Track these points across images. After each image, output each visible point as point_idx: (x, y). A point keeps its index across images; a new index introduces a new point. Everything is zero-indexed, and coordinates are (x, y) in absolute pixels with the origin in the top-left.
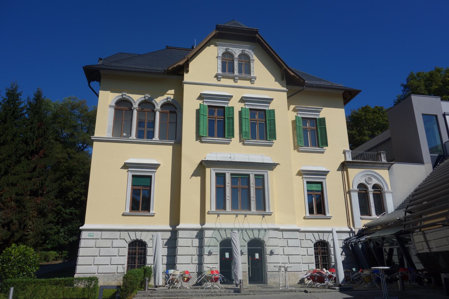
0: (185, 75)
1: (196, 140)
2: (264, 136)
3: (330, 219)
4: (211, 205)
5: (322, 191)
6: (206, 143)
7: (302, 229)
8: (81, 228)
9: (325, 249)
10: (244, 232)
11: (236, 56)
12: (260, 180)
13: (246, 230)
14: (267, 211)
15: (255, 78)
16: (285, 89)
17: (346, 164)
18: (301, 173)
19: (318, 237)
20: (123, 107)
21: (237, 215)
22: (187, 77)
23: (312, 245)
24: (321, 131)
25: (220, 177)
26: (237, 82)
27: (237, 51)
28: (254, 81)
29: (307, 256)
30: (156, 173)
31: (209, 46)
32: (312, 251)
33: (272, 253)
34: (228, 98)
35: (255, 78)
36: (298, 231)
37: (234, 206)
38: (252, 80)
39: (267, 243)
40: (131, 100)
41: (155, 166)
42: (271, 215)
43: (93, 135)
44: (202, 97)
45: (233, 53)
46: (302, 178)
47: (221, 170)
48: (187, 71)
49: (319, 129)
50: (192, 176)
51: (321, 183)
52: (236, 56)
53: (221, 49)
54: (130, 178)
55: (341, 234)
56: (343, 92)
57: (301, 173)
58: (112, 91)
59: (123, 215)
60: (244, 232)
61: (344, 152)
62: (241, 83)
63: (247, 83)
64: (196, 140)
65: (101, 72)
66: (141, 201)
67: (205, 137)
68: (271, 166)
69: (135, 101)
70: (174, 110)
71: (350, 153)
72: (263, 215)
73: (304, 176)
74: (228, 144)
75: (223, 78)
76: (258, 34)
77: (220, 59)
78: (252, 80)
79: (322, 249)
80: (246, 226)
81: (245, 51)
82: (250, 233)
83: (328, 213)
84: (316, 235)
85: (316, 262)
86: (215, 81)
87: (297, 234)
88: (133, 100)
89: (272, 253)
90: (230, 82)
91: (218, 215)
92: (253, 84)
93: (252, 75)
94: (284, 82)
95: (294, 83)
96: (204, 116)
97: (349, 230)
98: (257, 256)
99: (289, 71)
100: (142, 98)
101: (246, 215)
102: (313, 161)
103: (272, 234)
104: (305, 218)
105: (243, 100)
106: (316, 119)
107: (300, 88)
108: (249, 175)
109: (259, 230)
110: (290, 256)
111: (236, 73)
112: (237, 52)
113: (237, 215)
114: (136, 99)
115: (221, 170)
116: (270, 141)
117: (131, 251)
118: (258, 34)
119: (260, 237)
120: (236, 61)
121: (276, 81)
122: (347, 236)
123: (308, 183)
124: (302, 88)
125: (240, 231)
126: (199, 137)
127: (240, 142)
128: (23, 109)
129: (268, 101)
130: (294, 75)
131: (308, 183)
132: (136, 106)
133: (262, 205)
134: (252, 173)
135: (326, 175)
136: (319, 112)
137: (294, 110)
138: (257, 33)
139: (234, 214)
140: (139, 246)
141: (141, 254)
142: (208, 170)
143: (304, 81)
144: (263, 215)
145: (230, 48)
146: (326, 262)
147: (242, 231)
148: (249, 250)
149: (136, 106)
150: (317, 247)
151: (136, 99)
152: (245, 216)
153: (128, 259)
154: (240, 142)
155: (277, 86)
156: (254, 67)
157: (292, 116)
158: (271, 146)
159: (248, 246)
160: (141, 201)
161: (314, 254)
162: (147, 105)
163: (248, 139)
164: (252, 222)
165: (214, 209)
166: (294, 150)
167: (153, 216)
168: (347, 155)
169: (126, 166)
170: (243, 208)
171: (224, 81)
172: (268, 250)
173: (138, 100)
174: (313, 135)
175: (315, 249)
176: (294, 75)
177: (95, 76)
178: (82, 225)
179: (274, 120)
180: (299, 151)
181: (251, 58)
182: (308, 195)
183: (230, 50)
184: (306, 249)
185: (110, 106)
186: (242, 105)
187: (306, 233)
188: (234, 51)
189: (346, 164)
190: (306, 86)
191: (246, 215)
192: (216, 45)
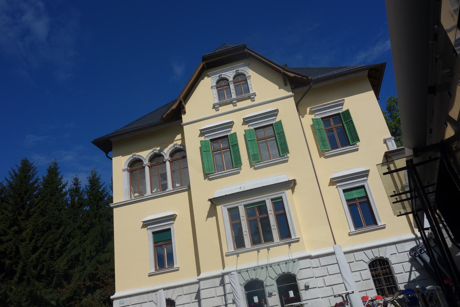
0: (183, 116)
1: (205, 179)
2: (346, 143)
3: (384, 228)
4: (229, 246)
5: (367, 197)
6: (214, 179)
7: (313, 254)
8: (112, 297)
9: (385, 268)
10: (269, 268)
11: (231, 79)
12: (279, 205)
13: (271, 265)
14: (293, 237)
15: (254, 94)
16: (291, 93)
17: (389, 155)
18: (334, 182)
19: (372, 255)
20: (135, 166)
21: (258, 250)
22: (185, 119)
23: (367, 266)
24: (348, 126)
25: (234, 214)
26: (236, 105)
27: (231, 73)
28: (254, 98)
29: (362, 281)
30: (174, 225)
31: (203, 79)
32: (367, 274)
33: (307, 288)
34: (230, 125)
35: (254, 94)
36: (310, 257)
37: (255, 241)
38: (251, 97)
39: (298, 277)
40: (141, 158)
41: (172, 218)
42: (298, 241)
43: (113, 202)
44: (203, 133)
45: (227, 77)
46: (337, 187)
47: (232, 205)
48: (185, 113)
49: (345, 125)
50: (207, 218)
51: (363, 187)
52: (231, 79)
53: (214, 78)
54: (151, 235)
55: (403, 244)
56: (366, 72)
57: (334, 182)
58: (123, 155)
59: (150, 275)
60: (269, 268)
61: (385, 142)
62: (240, 105)
63: (248, 103)
64: (205, 179)
65: (112, 140)
66: (164, 258)
67: (212, 173)
68: (290, 185)
69: (145, 157)
70: (180, 154)
71: (393, 141)
72: (289, 244)
73: (338, 185)
74: (238, 173)
75: (220, 106)
76: (247, 48)
77: (214, 89)
78: (251, 97)
79: (380, 269)
80: (272, 261)
81: (238, 70)
82: (277, 268)
83: (380, 221)
84: (368, 252)
85: (376, 287)
86: (214, 112)
87: (315, 262)
88: (143, 157)
89: (307, 288)
90: (230, 107)
91: (238, 254)
92: (254, 101)
93: (251, 92)
94: (289, 87)
95: (301, 85)
96: (208, 152)
97: (414, 236)
98: (256, 299)
99: (288, 73)
100: (151, 152)
101: (268, 248)
102: (345, 164)
103: (303, 264)
104: (350, 235)
105: (246, 121)
106: (339, 114)
107: (306, 88)
108: (264, 202)
109: (286, 262)
110: (333, 287)
111: (234, 96)
112: (230, 75)
113: (258, 250)
114: (145, 155)
115: (232, 205)
116: (354, 145)
117: (374, 272)
118: (247, 48)
119: (290, 271)
120: (231, 84)
121: (280, 88)
122: (413, 244)
123: (345, 191)
124: (309, 86)
125: (265, 269)
126: (207, 176)
127: (251, 167)
128: (66, 193)
129: (275, 113)
130: (294, 75)
131: (345, 191)
132: (146, 162)
133: (285, 232)
134: (268, 199)
135: (367, 176)
136: (342, 105)
137: (311, 113)
138: (245, 47)
139: (286, 244)
140: (381, 266)
141: (387, 274)
142: (219, 208)
143: (307, 77)
144: (289, 244)
145: (223, 74)
146: (391, 285)
147: (267, 267)
148: (279, 288)
149: (146, 162)
150: (374, 267)
151: (145, 155)
152: (268, 250)
153: (374, 281)
154: (251, 167)
155: (284, 93)
156: (252, 84)
157: (308, 119)
158: (287, 161)
159: (278, 284)
160: (164, 258)
161: (370, 277)
162: (156, 158)
163: (259, 162)
164: (277, 255)
165: (232, 249)
166: (320, 157)
167: (178, 270)
168: (389, 143)
169: (146, 224)
170: (368, 224)
171: (223, 109)
172: (301, 285)
173: (147, 156)
174: (339, 134)
175: (371, 271)
176: (294, 75)
177: (107, 146)
178: (113, 294)
179: (283, 132)
180: (326, 157)
181: (247, 75)
182: (349, 206)
183: (223, 76)
184: (358, 273)
185: (124, 170)
186: (246, 127)
187: (355, 253)
188: (228, 74)
189: (389, 155)
190: (314, 83)
191: (268, 248)
192: (209, 76)
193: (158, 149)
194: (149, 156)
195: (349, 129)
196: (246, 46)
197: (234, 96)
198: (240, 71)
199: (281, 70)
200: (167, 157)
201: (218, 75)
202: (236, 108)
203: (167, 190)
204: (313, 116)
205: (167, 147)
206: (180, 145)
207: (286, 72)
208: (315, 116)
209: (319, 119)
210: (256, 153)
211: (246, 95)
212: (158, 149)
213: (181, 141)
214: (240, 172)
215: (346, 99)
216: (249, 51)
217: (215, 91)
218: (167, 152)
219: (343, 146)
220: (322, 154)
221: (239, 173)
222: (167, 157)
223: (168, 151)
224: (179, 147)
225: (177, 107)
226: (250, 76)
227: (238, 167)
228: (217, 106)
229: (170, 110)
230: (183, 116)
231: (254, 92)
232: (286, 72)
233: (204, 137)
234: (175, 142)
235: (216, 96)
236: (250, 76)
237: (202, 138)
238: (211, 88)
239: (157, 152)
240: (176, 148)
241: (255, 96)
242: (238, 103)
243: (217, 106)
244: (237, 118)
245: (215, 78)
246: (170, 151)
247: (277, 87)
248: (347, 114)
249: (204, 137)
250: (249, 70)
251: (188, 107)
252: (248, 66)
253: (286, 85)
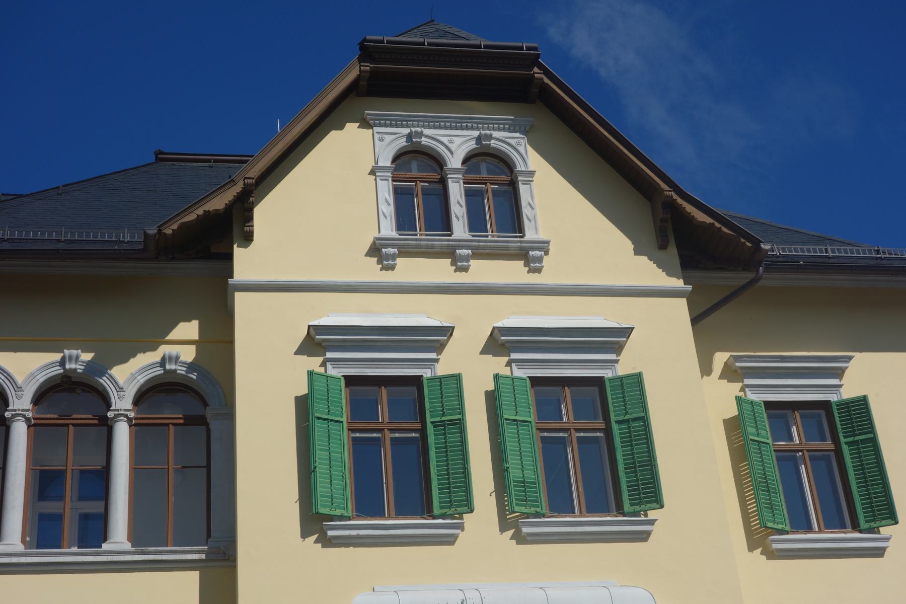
11: (455, 162)
15: (544, 246)
16: (677, 283)
22: (246, 264)
24: (858, 455)
28: (540, 260)
31: (341, 127)
34: (435, 338)
35: (544, 246)
38: (530, 255)
44: (316, 341)
45: (441, 149)
48: (248, 238)
52: (455, 162)
53: (388, 138)
62: (483, 271)
63: (511, 272)
67: (341, 518)
69: (20, 380)
74: (450, 540)
78: (530, 255)
86: (371, 271)
88: (9, 377)
90: (438, 270)
92: (538, 270)
96: (333, 426)
100: (51, 365)
105: (500, 342)
107: (741, 278)
111: (460, 229)
112: (455, 144)
118: (541, 67)
124: (751, 275)
126: (313, 522)
127: (503, 529)
129: (613, 339)
130: (709, 220)
138: (534, 60)
143: (757, 243)
154: (503, 529)
155: (648, 272)
156: (537, 203)
157: (721, 398)
163: (537, 515)
171: (409, 269)
173: (32, 376)
176: (709, 220)
179: (644, 420)
180: (772, 555)
181: (520, 167)
186: (498, 364)
190: (767, 269)
192: (365, 124)
193: (87, 357)
194: (41, 378)
195: (861, 468)
196: (538, 56)
197: (460, 229)
198: (424, 141)
199: (663, 185)
200: (122, 403)
201: (406, 131)
202: (388, 277)
203: (105, 546)
204: (734, 388)
205: (126, 361)
206: (191, 367)
207: (680, 201)
208: (323, 364)
209: (758, 404)
210: (529, 475)
211: (513, 241)
212: (87, 357)
213: (193, 347)
214: (455, 537)
215: (857, 355)
216: (546, 80)
217: (386, 189)
218: (127, 377)
219: (401, 512)
220: (758, 538)
221: (452, 543)
222: (122, 403)
223: (133, 377)
224: (182, 370)
225: (229, 208)
226: (532, 173)
227: (452, 517)
228: (391, 251)
229: (200, 212)
230: (238, 252)
231: (542, 236)
232: (680, 201)
233: (320, 360)
234: (165, 349)
235: (389, 209)
236: (532, 173)
237: (314, 363)
238: (372, 172)
239: (80, 368)
240: (167, 372)
241: (547, 253)
242: (400, 261)
243: (391, 251)
244: (467, 321)
245: (388, 142)
246: (142, 379)
247: (628, 245)
248: (858, 412)
249: (320, 360)
250: (529, 148)
251: (266, 214)
252: (525, 132)
253: (663, 246)
